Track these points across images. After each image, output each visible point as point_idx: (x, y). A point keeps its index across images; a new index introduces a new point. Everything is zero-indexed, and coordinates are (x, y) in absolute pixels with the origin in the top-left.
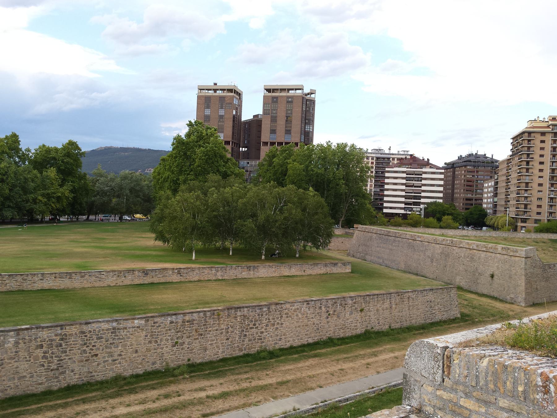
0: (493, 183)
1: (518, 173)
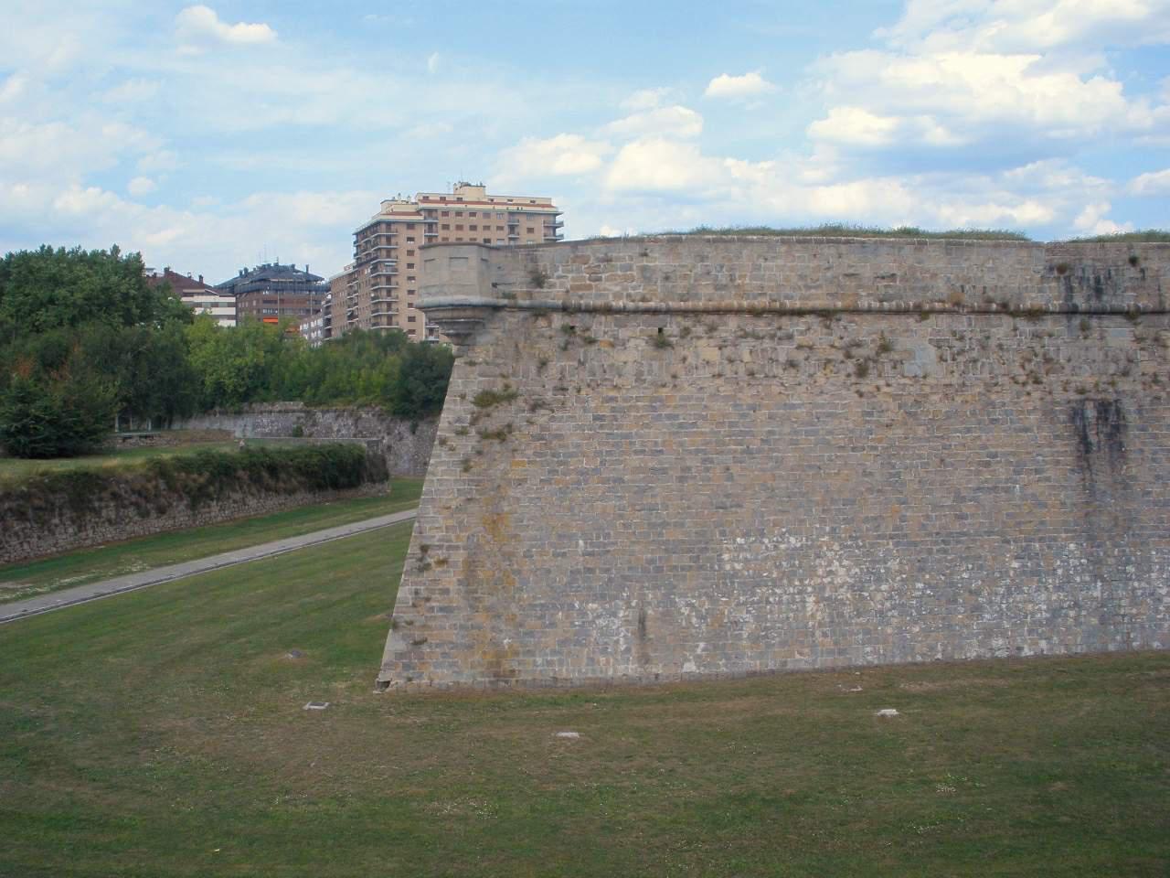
0: (320, 322)
1: (373, 299)
